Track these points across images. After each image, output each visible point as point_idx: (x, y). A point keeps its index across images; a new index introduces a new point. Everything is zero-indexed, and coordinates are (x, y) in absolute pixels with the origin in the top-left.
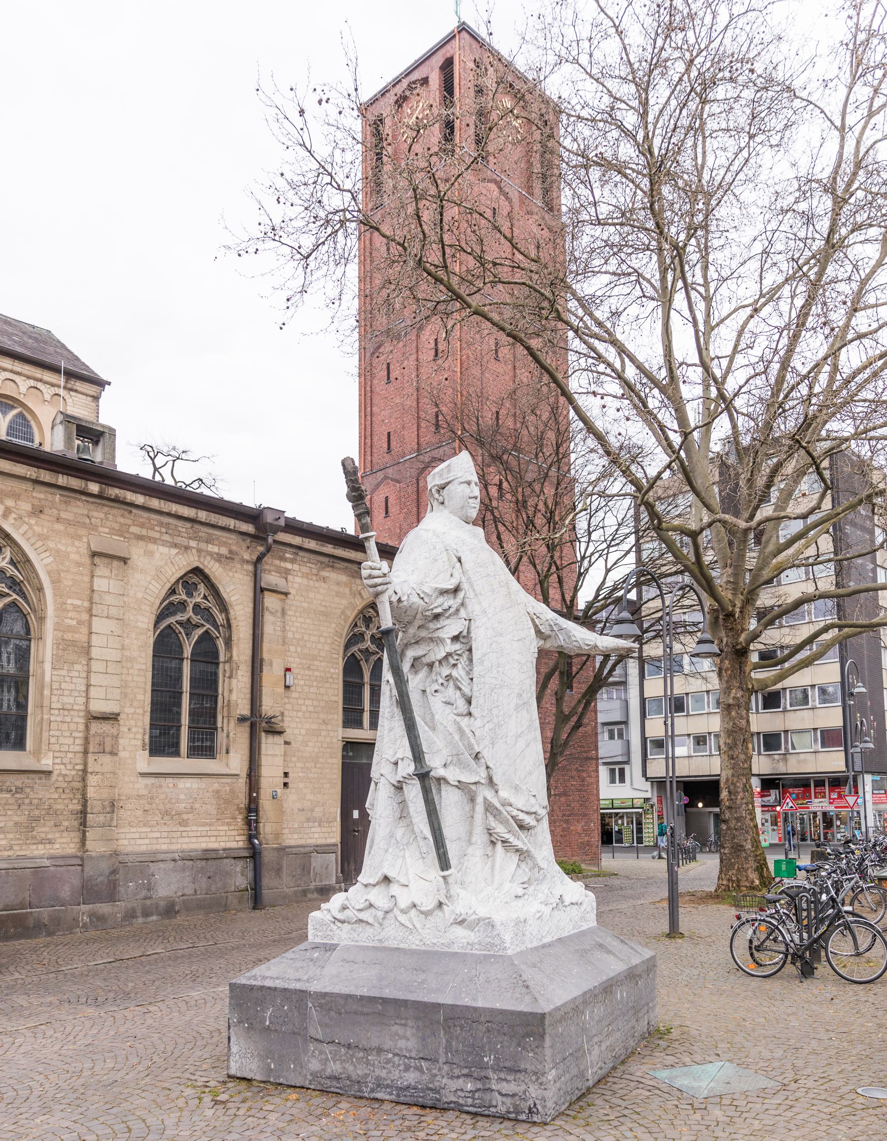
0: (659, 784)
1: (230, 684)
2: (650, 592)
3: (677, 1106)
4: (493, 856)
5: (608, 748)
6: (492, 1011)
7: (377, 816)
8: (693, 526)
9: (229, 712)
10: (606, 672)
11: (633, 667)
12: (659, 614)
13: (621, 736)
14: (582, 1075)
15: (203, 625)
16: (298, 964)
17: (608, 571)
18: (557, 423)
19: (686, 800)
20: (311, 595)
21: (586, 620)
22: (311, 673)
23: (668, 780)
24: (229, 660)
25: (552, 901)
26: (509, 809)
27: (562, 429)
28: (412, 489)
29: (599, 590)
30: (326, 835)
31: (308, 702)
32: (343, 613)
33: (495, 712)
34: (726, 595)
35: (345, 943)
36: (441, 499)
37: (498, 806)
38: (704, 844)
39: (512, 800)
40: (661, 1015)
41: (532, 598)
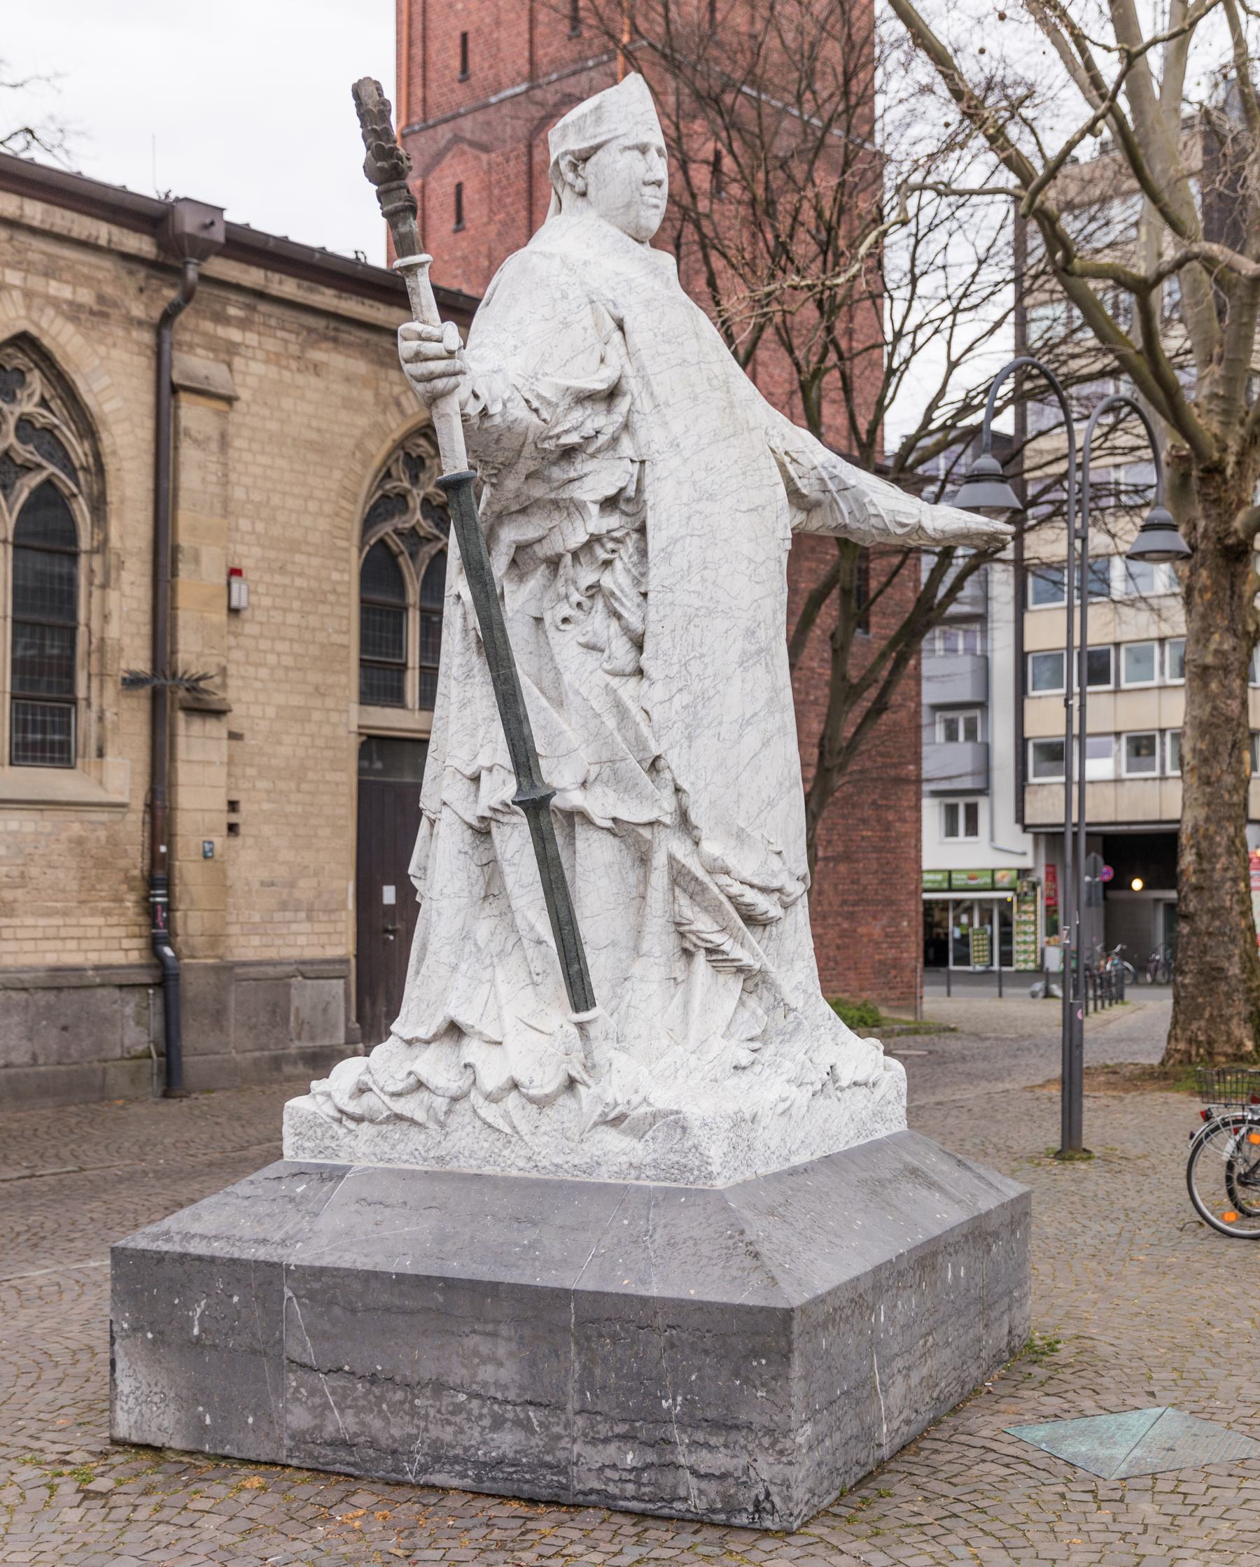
0: (1051, 839)
1: (103, 601)
2: (1044, 415)
3: (1063, 1496)
4: (687, 981)
5: (943, 758)
6: (680, 1305)
7: (435, 894)
8: (1142, 269)
9: (102, 663)
10: (942, 591)
11: (1001, 581)
12: (1061, 467)
13: (971, 734)
14: (867, 1435)
15: (39, 467)
16: (262, 1209)
17: (953, 365)
18: (848, 23)
19: (1107, 873)
20: (287, 403)
21: (904, 473)
22: (287, 580)
23: (1069, 831)
24: (102, 548)
25: (813, 1076)
26: (724, 880)
27: (858, 38)
28: (516, 168)
29: (933, 406)
30: (324, 939)
31: (282, 646)
32: (359, 446)
33: (695, 668)
34: (1208, 424)
35: (364, 1163)
36: (579, 184)
37: (700, 873)
38: (1141, 968)
39: (731, 862)
40: (1037, 1315)
41: (780, 418)
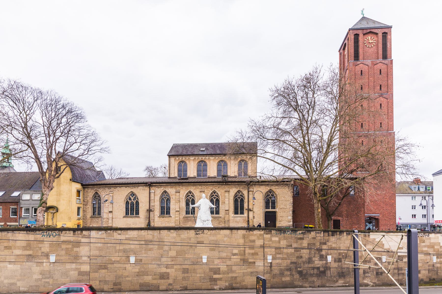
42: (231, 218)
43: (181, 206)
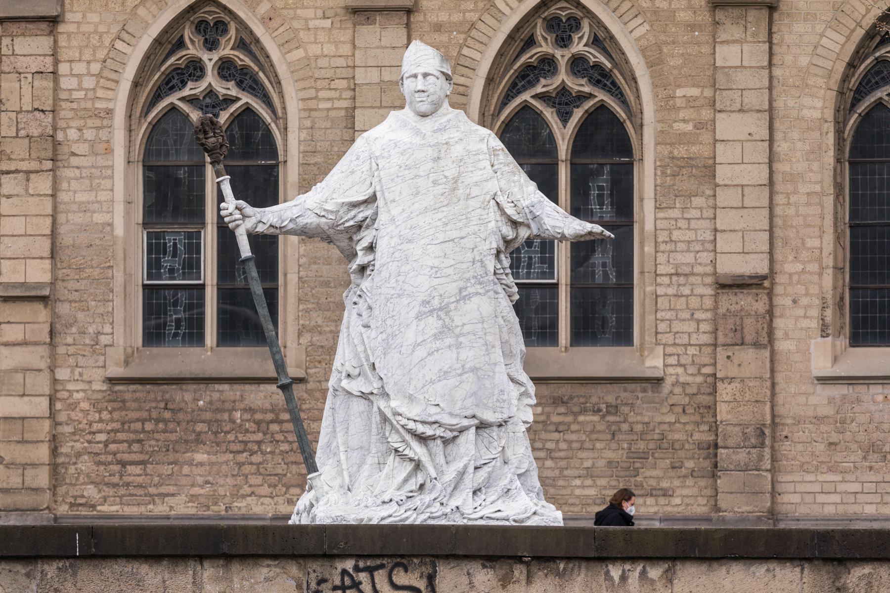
15: (590, 96)
26: (400, 418)
33: (389, 322)
42: (802, 400)
43: (71, 221)
